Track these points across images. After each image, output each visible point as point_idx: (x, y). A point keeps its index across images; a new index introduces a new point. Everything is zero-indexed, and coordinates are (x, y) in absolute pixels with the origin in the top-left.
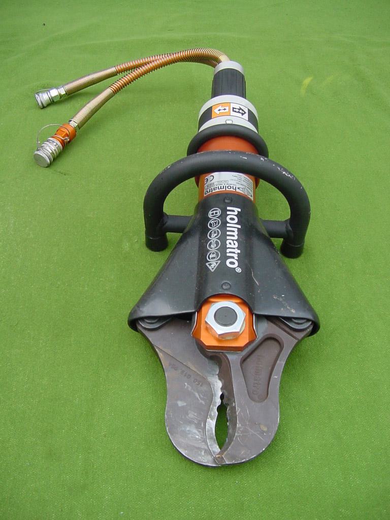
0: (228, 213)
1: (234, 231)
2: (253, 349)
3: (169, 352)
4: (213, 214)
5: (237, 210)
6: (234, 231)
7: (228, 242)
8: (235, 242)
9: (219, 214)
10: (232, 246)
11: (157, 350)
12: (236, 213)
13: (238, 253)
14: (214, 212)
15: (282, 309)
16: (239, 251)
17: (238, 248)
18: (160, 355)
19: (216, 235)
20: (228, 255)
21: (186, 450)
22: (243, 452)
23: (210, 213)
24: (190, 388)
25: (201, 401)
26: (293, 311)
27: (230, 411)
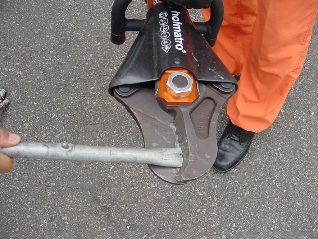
0: (172, 15)
1: (178, 27)
2: (194, 108)
3: (140, 110)
4: (162, 15)
5: (178, 13)
6: (178, 27)
7: (175, 33)
8: (180, 33)
9: (166, 16)
10: (178, 36)
11: (132, 110)
12: (178, 15)
13: (182, 41)
14: (163, 14)
15: (215, 77)
16: (183, 40)
17: (182, 37)
18: (135, 113)
19: (166, 29)
20: (176, 41)
21: (163, 175)
22: (194, 173)
23: (160, 15)
24: (159, 134)
25: (168, 142)
26: (222, 78)
27: (184, 146)
